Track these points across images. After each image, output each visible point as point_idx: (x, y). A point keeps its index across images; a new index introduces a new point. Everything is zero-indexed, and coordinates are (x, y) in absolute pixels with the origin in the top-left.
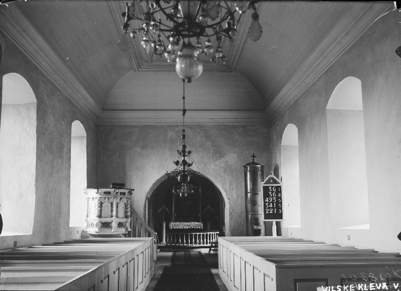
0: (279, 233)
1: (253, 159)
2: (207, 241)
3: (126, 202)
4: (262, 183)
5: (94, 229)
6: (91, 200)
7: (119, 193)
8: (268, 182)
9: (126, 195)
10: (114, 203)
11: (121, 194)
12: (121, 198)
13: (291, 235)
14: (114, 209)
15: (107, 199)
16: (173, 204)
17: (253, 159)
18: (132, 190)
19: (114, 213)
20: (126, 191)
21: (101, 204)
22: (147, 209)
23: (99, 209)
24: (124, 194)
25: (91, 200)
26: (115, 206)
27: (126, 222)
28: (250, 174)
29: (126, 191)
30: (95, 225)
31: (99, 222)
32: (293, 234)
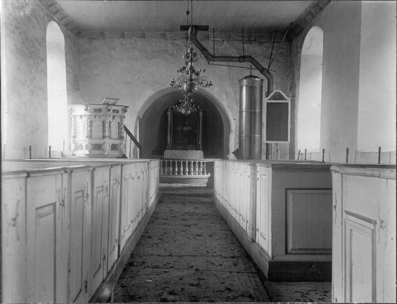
0: (267, 158)
1: (251, 72)
2: (194, 170)
3: (120, 121)
4: (265, 98)
5: (83, 151)
6: (78, 118)
7: (111, 110)
8: (274, 98)
9: (120, 112)
10: (107, 121)
11: (114, 111)
12: (114, 116)
13: (336, 300)
14: (107, 129)
15: (97, 117)
16: (201, 117)
17: (251, 72)
18: (126, 107)
19: (107, 133)
20: (120, 109)
21: (91, 123)
22: (138, 130)
23: (89, 128)
24: (118, 111)
25: (78, 118)
26: (107, 125)
27: (121, 144)
28: (246, 88)
29: (120, 109)
30: (84, 148)
31: (89, 144)
32: (338, 300)
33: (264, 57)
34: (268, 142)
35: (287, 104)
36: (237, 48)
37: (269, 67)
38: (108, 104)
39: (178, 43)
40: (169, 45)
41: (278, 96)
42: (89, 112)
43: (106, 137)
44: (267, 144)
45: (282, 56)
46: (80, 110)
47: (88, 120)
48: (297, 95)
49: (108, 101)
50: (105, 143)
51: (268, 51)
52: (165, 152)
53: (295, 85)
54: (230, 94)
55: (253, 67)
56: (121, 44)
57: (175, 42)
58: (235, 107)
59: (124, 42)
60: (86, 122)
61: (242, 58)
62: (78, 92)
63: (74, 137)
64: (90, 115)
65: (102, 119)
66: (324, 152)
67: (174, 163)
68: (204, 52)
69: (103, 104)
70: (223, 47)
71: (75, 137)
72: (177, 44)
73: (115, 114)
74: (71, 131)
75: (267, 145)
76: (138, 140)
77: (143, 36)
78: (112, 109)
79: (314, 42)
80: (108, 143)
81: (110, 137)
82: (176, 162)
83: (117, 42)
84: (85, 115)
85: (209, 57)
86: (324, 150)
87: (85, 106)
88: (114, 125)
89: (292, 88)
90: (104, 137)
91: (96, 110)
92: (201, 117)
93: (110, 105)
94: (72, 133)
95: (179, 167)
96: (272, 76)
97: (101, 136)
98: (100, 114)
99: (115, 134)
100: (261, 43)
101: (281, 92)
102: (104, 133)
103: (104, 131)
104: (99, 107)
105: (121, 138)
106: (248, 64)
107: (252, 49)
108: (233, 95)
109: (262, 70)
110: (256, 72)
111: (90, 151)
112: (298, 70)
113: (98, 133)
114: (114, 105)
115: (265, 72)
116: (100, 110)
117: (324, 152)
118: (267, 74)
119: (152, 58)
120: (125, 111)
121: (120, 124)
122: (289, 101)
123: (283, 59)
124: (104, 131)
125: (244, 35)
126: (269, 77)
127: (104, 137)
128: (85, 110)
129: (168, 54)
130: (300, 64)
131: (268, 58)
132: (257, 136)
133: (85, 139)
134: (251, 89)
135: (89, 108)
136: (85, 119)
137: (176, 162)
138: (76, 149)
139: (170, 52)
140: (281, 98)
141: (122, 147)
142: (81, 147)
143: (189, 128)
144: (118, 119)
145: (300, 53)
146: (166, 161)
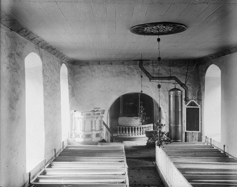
1: (175, 86)
8: (191, 105)
10: (94, 121)
11: (97, 114)
16: (139, 97)
19: (94, 128)
20: (100, 112)
21: (85, 122)
23: (83, 126)
27: (101, 133)
29: (100, 112)
30: (81, 137)
33: (182, 75)
34: (187, 131)
35: (198, 109)
36: (166, 70)
37: (186, 83)
38: (94, 111)
39: (131, 67)
40: (126, 68)
41: (192, 104)
42: (84, 116)
43: (93, 130)
44: (186, 133)
45: (192, 74)
46: (78, 115)
47: (83, 121)
48: (203, 100)
49: (94, 109)
50: (93, 134)
51: (184, 71)
52: (119, 119)
53: (201, 93)
54: (161, 96)
55: (176, 83)
56: (98, 68)
57: (130, 66)
58: (165, 105)
59: (100, 67)
60: (82, 122)
61: (170, 78)
62: (74, 98)
63: (74, 130)
64: (84, 118)
65: (91, 119)
66: (224, 147)
67: (126, 128)
68: (148, 75)
69: (91, 111)
70: (157, 69)
71: (75, 130)
72: (131, 68)
73: (98, 116)
74: (73, 123)
75: (186, 133)
76: (109, 127)
77: (111, 64)
78: (96, 113)
79: (213, 72)
80: (94, 133)
81: (95, 130)
82: (127, 128)
83: (95, 67)
84: (81, 118)
85: (151, 78)
86: (224, 146)
87: (81, 113)
88: (98, 122)
89: (199, 96)
90: (92, 130)
91: (87, 114)
92: (139, 97)
93: (95, 111)
94: (73, 127)
95: (129, 132)
96: (187, 88)
97: (90, 130)
98: (89, 117)
99: (98, 128)
100: (180, 67)
101: (195, 101)
102: (92, 128)
103: (92, 127)
104: (89, 113)
105: (101, 129)
106: (173, 81)
107: (175, 70)
108: (164, 98)
109: (182, 85)
110: (178, 86)
111: (84, 140)
112: (203, 85)
113: (88, 127)
114: (97, 111)
115: (183, 86)
116: (90, 114)
117: (224, 147)
118: (185, 87)
119: (116, 76)
120: (103, 113)
121: (100, 121)
122: (199, 107)
123: (193, 75)
124: (92, 127)
125: (170, 62)
126: (186, 89)
127: (92, 130)
128: (81, 115)
129: (126, 74)
130: (204, 82)
131: (185, 75)
132: (180, 125)
133: (81, 132)
134: (176, 97)
135: (83, 114)
136: (81, 120)
137: (127, 128)
138: (76, 137)
139: (127, 73)
140: (195, 105)
141: (102, 135)
142: (78, 136)
143: (132, 103)
144: (99, 118)
145: (204, 75)
146: (121, 127)
